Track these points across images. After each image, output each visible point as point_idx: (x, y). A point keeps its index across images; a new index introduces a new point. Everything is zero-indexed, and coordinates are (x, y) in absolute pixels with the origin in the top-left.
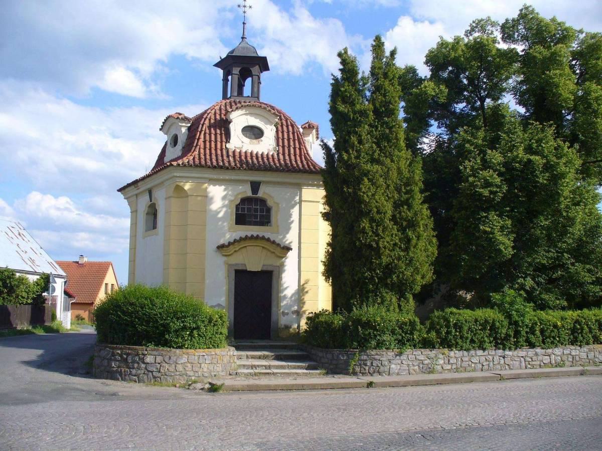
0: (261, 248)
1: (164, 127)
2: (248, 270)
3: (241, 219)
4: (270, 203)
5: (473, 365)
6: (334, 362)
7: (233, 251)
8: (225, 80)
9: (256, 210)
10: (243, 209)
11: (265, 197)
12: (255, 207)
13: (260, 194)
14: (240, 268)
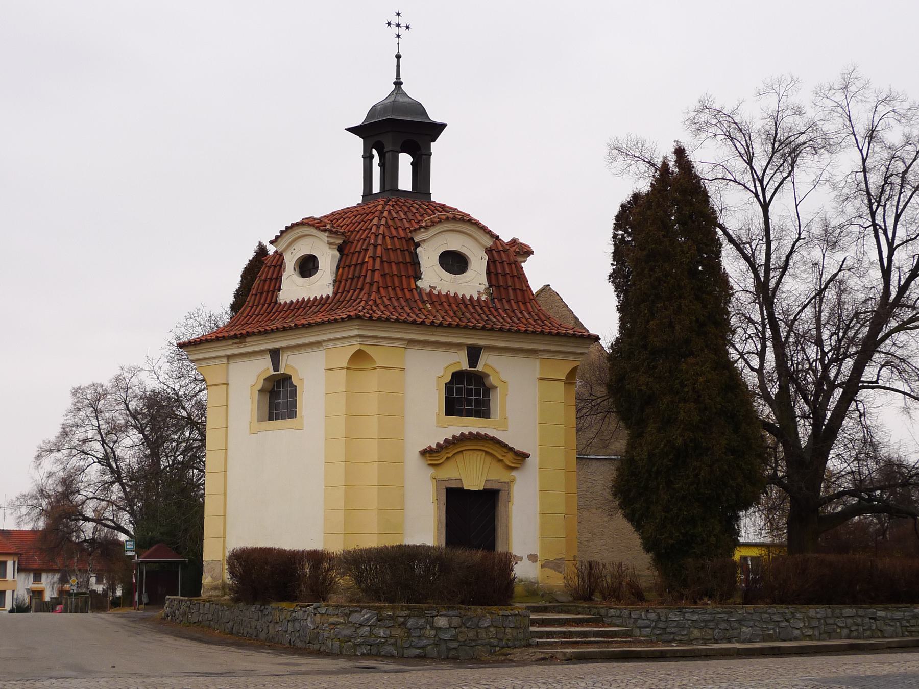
0: (484, 453)
1: (279, 240)
2: (465, 489)
3: (452, 408)
4: (493, 380)
5: (839, 630)
6: (661, 625)
7: (445, 458)
8: (368, 158)
9: (469, 392)
10: (459, 391)
11: (487, 371)
12: (468, 387)
13: (480, 367)
14: (454, 485)
